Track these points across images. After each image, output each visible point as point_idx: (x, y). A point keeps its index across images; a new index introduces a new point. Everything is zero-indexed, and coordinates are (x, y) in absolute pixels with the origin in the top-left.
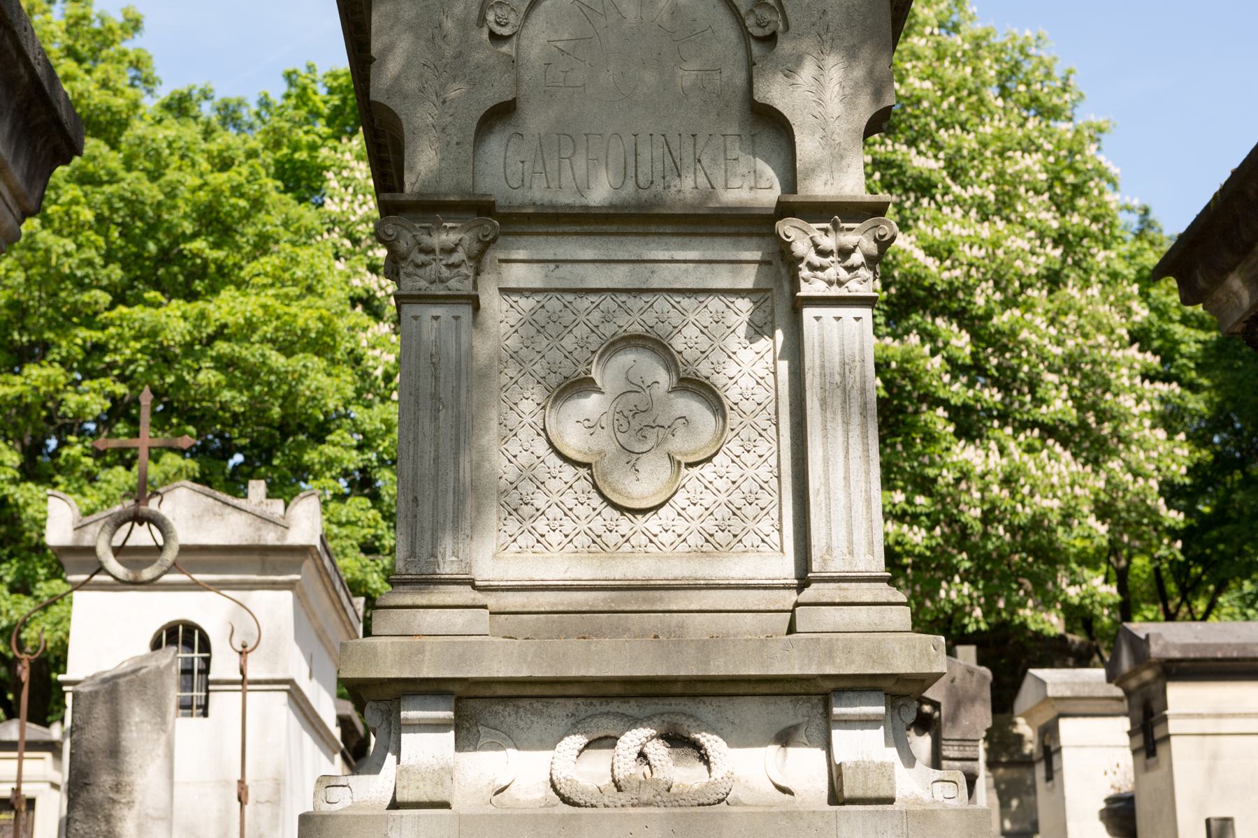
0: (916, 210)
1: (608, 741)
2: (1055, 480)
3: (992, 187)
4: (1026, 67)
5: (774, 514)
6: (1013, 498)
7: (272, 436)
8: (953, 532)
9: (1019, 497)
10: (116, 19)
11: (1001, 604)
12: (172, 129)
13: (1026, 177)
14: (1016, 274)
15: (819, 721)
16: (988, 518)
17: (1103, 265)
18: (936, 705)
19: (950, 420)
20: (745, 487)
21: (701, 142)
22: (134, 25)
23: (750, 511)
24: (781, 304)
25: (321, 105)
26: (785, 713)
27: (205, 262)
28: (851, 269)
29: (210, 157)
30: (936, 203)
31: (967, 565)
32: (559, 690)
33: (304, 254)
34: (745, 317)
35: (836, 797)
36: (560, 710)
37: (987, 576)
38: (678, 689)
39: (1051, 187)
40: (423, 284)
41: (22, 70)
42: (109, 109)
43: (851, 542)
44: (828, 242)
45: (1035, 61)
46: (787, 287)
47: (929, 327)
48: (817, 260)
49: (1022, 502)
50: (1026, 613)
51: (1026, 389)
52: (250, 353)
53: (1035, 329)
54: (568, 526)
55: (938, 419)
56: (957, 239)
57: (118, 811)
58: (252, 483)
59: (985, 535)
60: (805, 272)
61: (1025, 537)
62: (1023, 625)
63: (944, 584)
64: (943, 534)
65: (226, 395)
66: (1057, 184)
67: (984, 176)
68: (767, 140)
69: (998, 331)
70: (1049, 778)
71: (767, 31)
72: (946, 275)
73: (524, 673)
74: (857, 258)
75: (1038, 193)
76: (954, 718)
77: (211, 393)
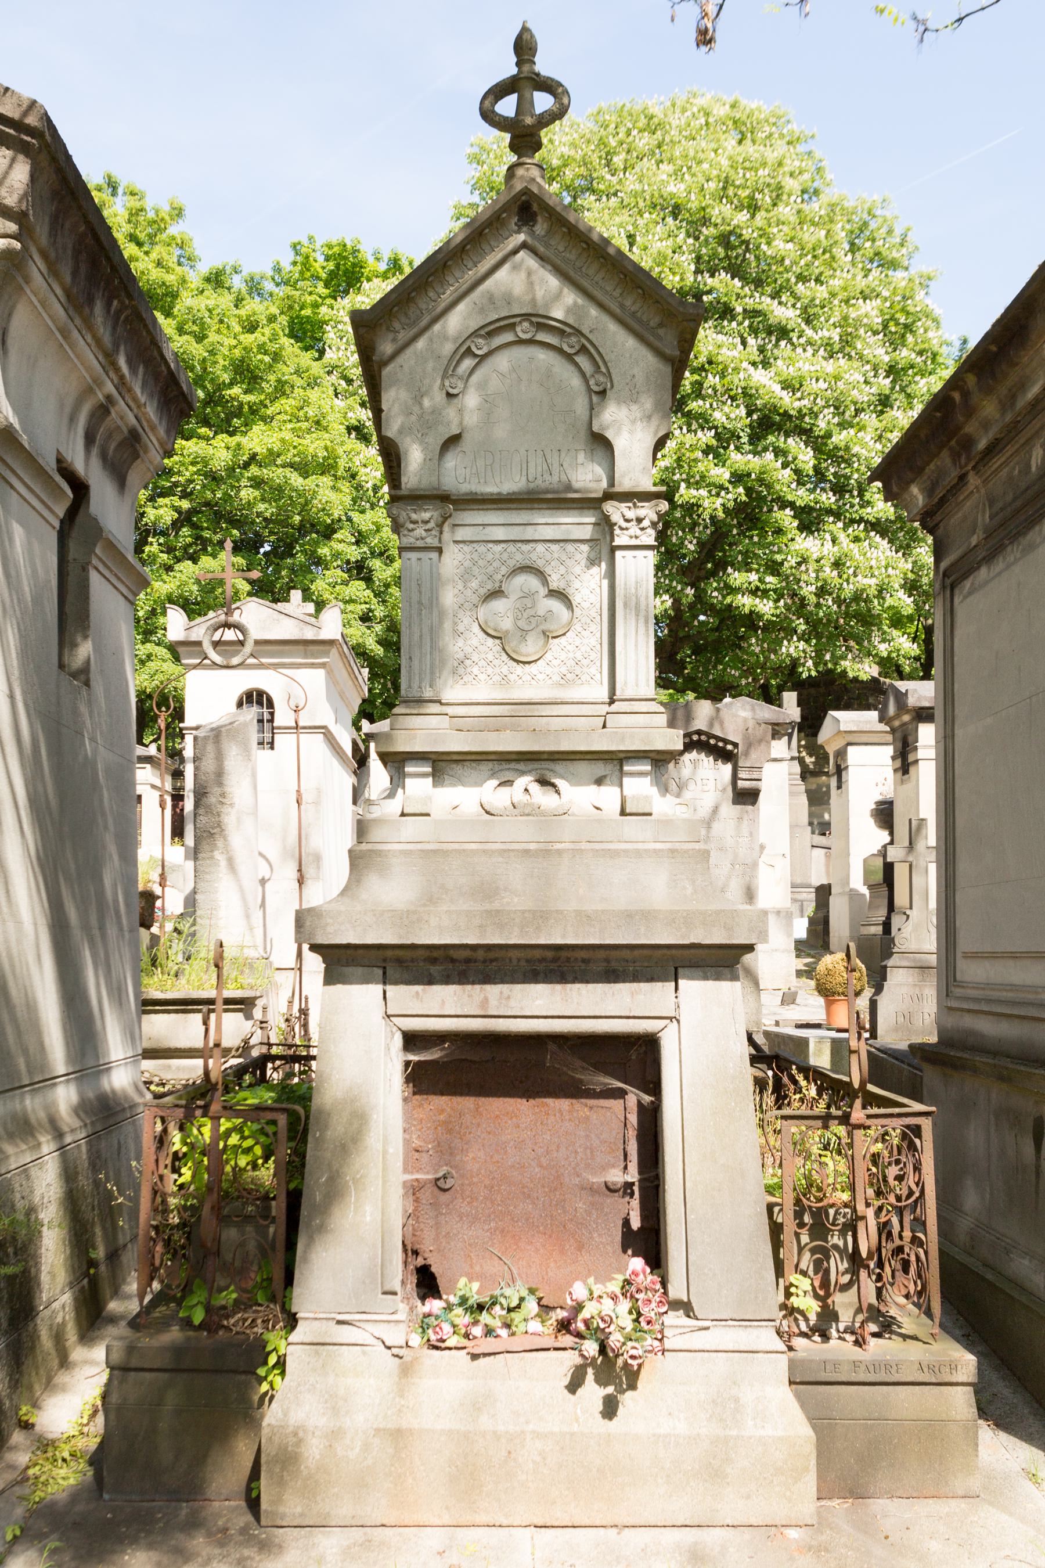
0: (775, 351)
1: (508, 783)
2: (873, 563)
3: (838, 330)
4: (873, 225)
5: (598, 664)
6: (840, 577)
7: (293, 535)
8: (794, 603)
9: (845, 576)
10: (165, 209)
11: (828, 657)
12: (212, 299)
13: (865, 321)
14: (852, 402)
15: (617, 773)
16: (822, 591)
17: (925, 389)
18: (736, 745)
19: (794, 517)
20: (583, 649)
21: (563, 455)
22: (178, 213)
23: (585, 662)
24: (604, 547)
25: (320, 270)
26: (600, 769)
27: (241, 405)
28: (642, 529)
29: (240, 321)
30: (793, 344)
31: (803, 627)
32: (484, 757)
33: (313, 395)
34: (585, 555)
35: (623, 813)
36: (485, 767)
37: (818, 636)
38: (545, 756)
39: (885, 326)
40: (412, 540)
41: (163, 368)
42: (164, 283)
43: (637, 680)
44: (631, 514)
45: (880, 220)
46: (608, 538)
47: (782, 445)
48: (624, 525)
49: (847, 581)
50: (845, 664)
51: (856, 493)
52: (276, 474)
53: (864, 445)
54: (490, 670)
55: (785, 518)
56: (807, 375)
57: (225, 809)
58: (292, 592)
59: (818, 605)
60: (617, 531)
61: (848, 606)
62: (844, 672)
63: (785, 642)
64: (786, 604)
65: (261, 507)
66: (892, 323)
67: (831, 322)
68: (600, 453)
69: (836, 448)
70: (839, 787)
71: (601, 388)
72: (797, 404)
73: (466, 749)
74: (646, 523)
75: (875, 333)
76: (747, 754)
77: (250, 505)
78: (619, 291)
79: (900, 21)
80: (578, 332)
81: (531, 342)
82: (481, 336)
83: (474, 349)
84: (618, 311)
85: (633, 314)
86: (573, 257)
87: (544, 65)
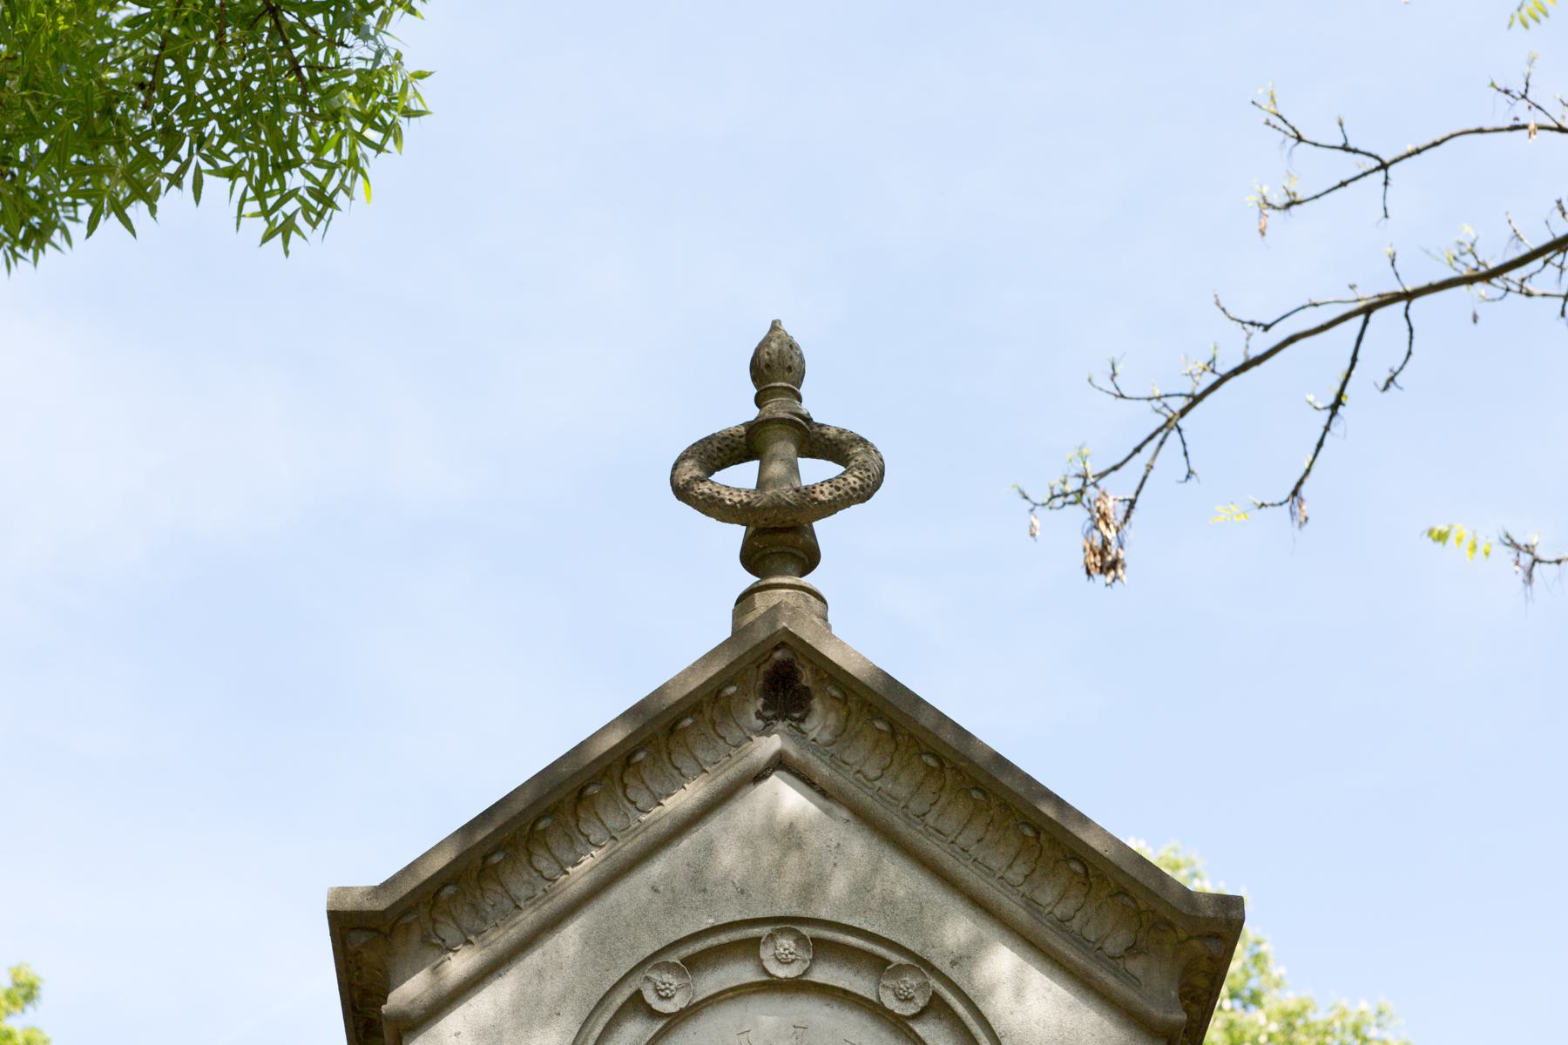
78: (1020, 870)
79: (1482, 548)
80: (922, 964)
81: (799, 987)
82: (670, 967)
83: (650, 997)
84: (1022, 915)
85: (1062, 923)
86: (902, 792)
87: (821, 402)
